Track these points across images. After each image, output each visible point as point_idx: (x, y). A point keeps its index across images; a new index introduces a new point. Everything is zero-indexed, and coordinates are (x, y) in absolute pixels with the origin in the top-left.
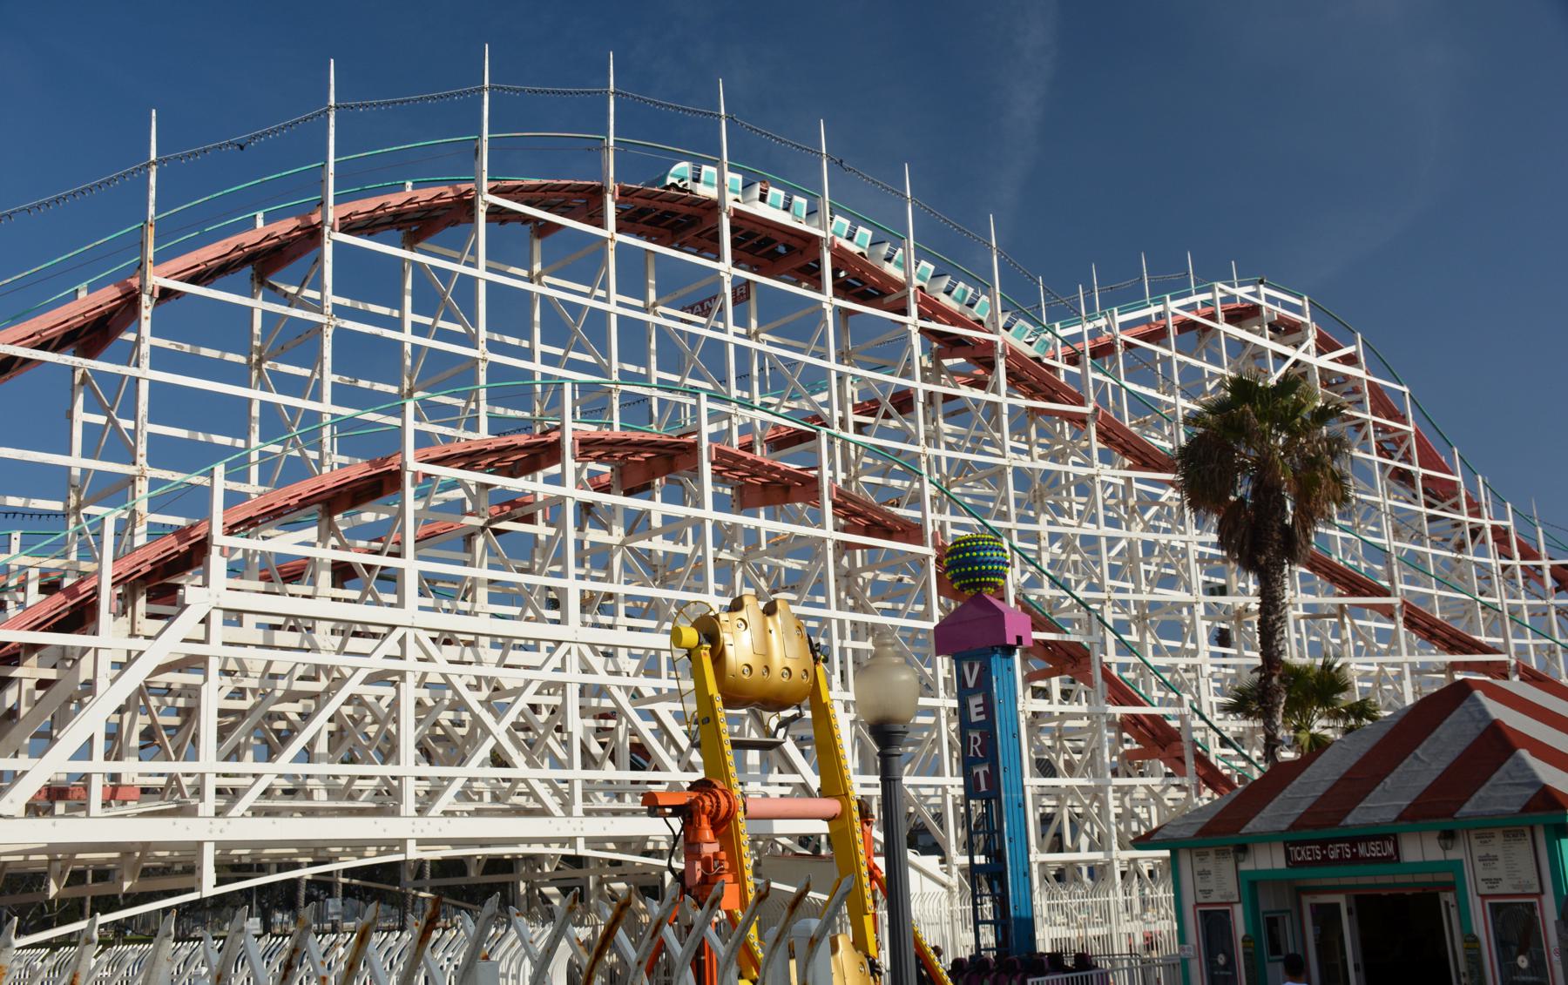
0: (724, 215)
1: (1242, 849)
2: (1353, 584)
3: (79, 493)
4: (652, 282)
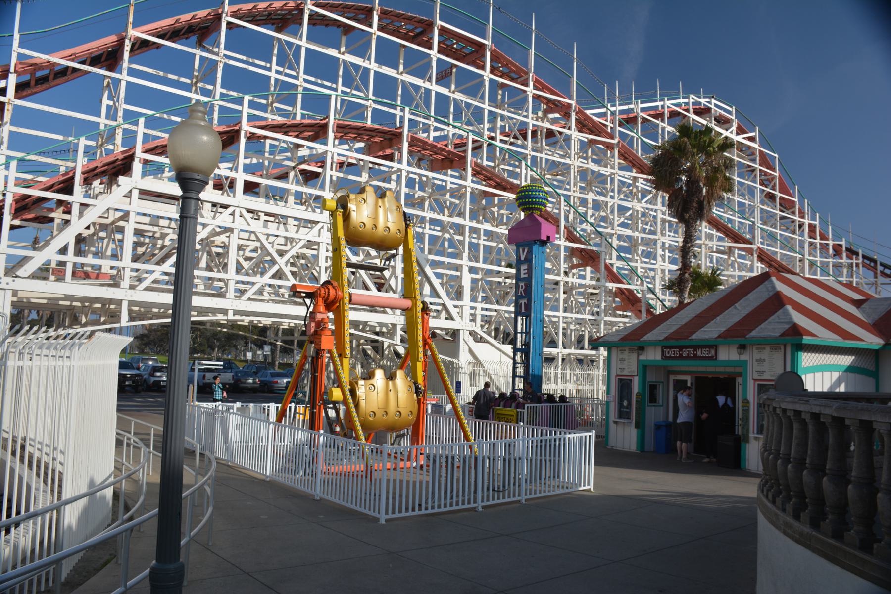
0: (436, 28)
1: (642, 349)
2: (736, 237)
3: (102, 138)
4: (402, 61)
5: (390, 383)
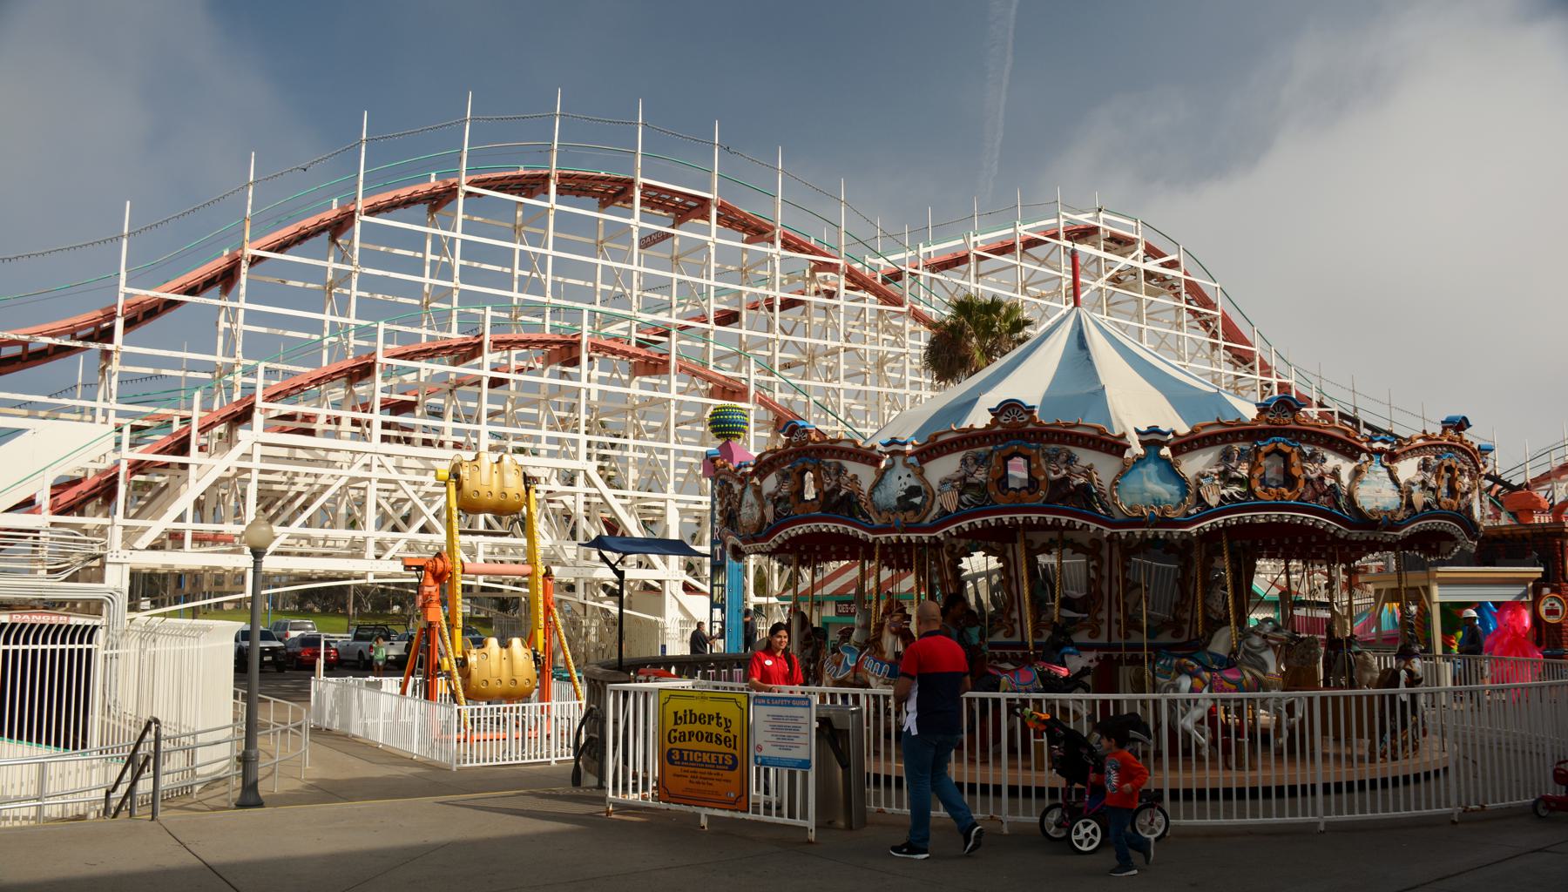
0: (636, 188)
5: (504, 650)
